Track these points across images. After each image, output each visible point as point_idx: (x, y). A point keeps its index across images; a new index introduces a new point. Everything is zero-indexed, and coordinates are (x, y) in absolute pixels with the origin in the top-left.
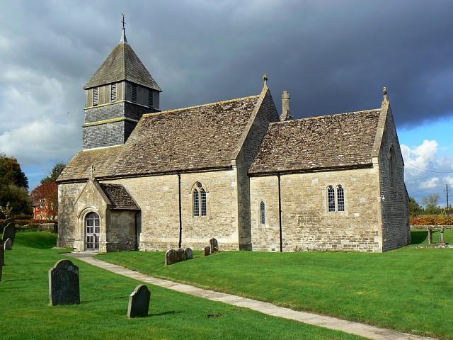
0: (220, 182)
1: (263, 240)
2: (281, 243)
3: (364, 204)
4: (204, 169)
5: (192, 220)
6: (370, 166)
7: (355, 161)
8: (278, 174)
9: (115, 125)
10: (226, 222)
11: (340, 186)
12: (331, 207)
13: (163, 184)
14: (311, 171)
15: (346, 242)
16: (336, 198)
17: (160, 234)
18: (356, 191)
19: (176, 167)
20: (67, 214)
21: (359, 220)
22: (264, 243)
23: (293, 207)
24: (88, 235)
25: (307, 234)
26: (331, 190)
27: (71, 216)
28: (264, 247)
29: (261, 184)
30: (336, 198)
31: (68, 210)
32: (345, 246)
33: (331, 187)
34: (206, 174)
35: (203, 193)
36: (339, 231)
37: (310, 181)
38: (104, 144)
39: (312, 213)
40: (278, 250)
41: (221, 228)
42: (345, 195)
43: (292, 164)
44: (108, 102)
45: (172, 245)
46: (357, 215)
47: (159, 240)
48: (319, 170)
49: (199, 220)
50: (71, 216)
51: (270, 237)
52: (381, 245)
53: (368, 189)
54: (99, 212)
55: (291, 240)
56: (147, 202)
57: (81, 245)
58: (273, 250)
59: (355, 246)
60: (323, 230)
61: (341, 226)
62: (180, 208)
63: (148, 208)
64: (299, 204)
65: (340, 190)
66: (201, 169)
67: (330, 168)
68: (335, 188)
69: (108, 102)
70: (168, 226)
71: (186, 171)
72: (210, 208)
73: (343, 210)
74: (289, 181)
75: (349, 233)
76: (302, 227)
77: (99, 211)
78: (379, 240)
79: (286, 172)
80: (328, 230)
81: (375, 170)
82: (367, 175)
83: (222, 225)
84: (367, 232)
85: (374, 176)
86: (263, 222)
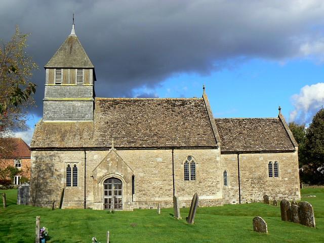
0: (207, 157)
1: (226, 196)
2: (240, 198)
3: (290, 173)
4: (195, 147)
5: (183, 183)
6: (293, 151)
7: (285, 148)
8: (238, 153)
9: (85, 104)
10: (212, 185)
11: (75, 166)
12: (271, 175)
13: (157, 156)
14: (259, 152)
15: (281, 195)
16: (273, 170)
17: (153, 195)
18: (286, 165)
19: (168, 144)
20: (43, 178)
21: (288, 182)
22: (227, 198)
23: (247, 174)
24: (106, 197)
25: (257, 192)
26: (270, 164)
27: (48, 181)
28: (228, 201)
29: (225, 159)
30: (273, 170)
31: (45, 175)
32: (280, 197)
33: (69, 166)
34: (196, 150)
35: (193, 166)
36: (276, 189)
37: (258, 159)
38: (71, 118)
39: (260, 178)
40: (237, 202)
41: (209, 189)
42: (78, 176)
43: (130, 142)
44: (74, 83)
45: (166, 203)
46: (286, 179)
47: (152, 199)
48: (265, 152)
49: (190, 183)
50: (48, 181)
51: (232, 194)
52: (300, 197)
53: (292, 164)
54: (125, 178)
55: (246, 195)
56: (141, 170)
57: (102, 207)
58: (234, 202)
59: (285, 197)
60: (267, 188)
61: (278, 186)
62: (173, 174)
63: (142, 175)
64: (251, 173)
65: (276, 164)
66: (192, 147)
67: (270, 151)
68: (273, 163)
69: (74, 83)
70: (161, 189)
71: (179, 148)
72: (200, 175)
73: (185, 180)
74: (245, 158)
75: (282, 190)
76: (253, 187)
77: (125, 178)
78: (299, 193)
79: (242, 152)
80: (270, 188)
81: (296, 154)
82: (283, 156)
83: (209, 186)
84: (292, 189)
85: (295, 157)
86: (225, 184)
